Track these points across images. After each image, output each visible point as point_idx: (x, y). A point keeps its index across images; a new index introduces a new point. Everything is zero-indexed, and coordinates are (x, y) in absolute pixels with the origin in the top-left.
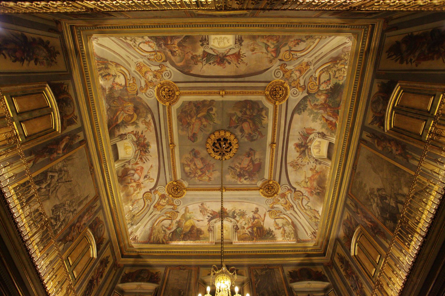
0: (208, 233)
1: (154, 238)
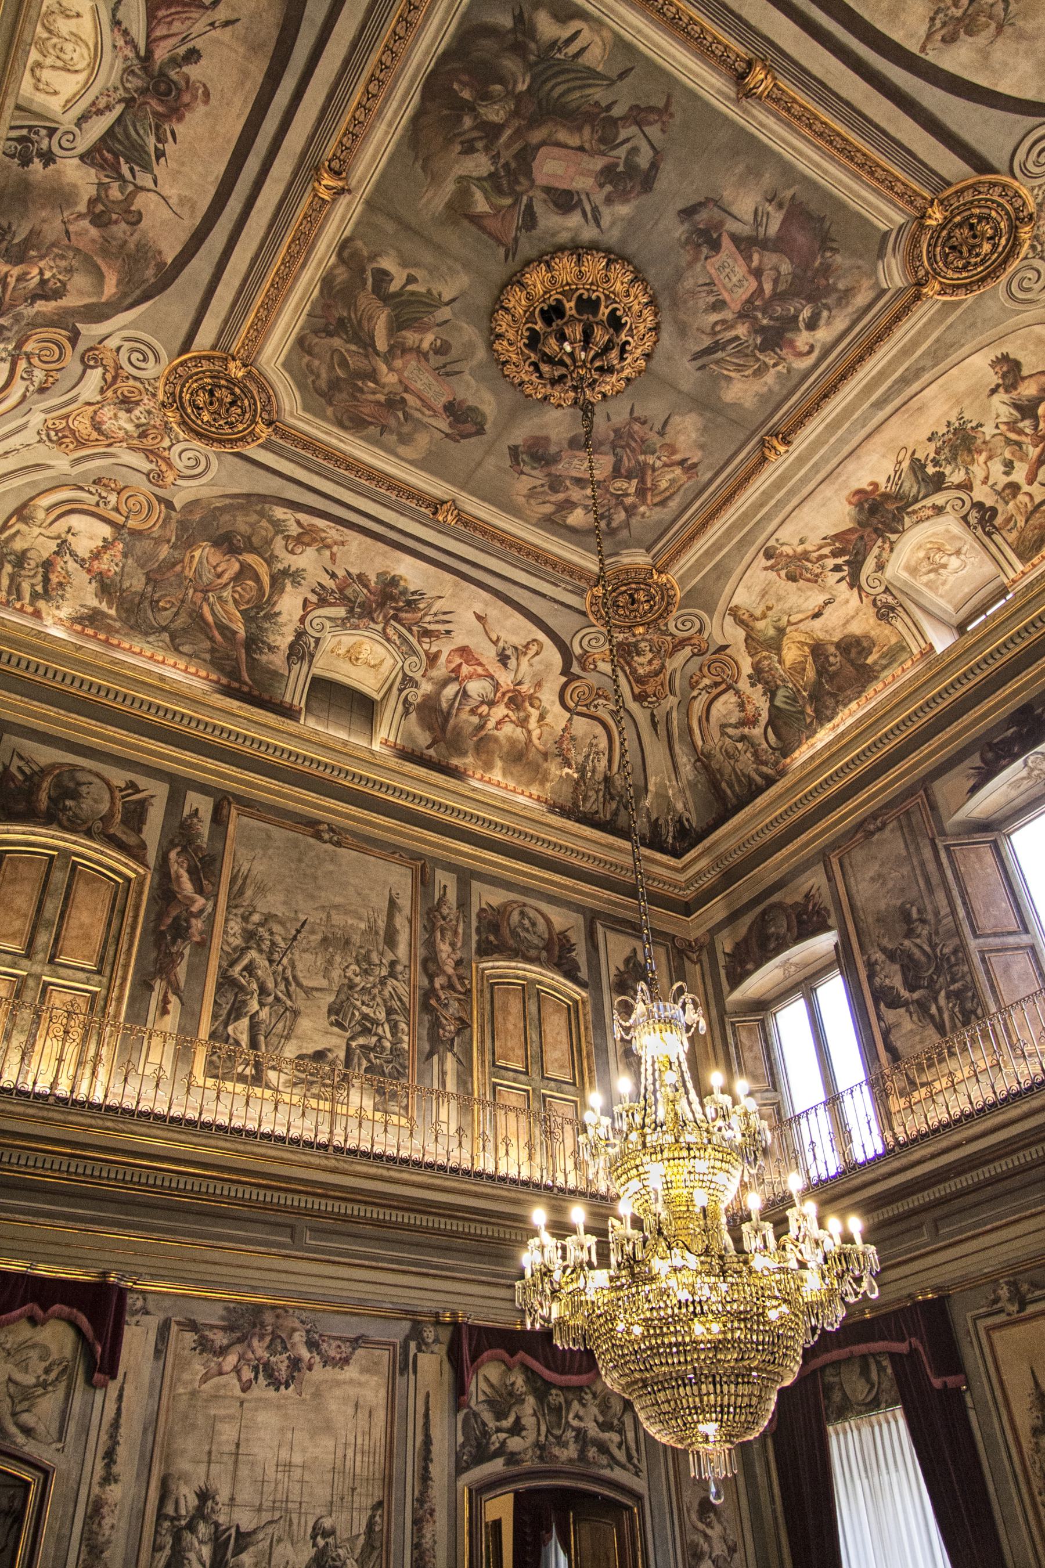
0: (887, 630)
1: (731, 786)
